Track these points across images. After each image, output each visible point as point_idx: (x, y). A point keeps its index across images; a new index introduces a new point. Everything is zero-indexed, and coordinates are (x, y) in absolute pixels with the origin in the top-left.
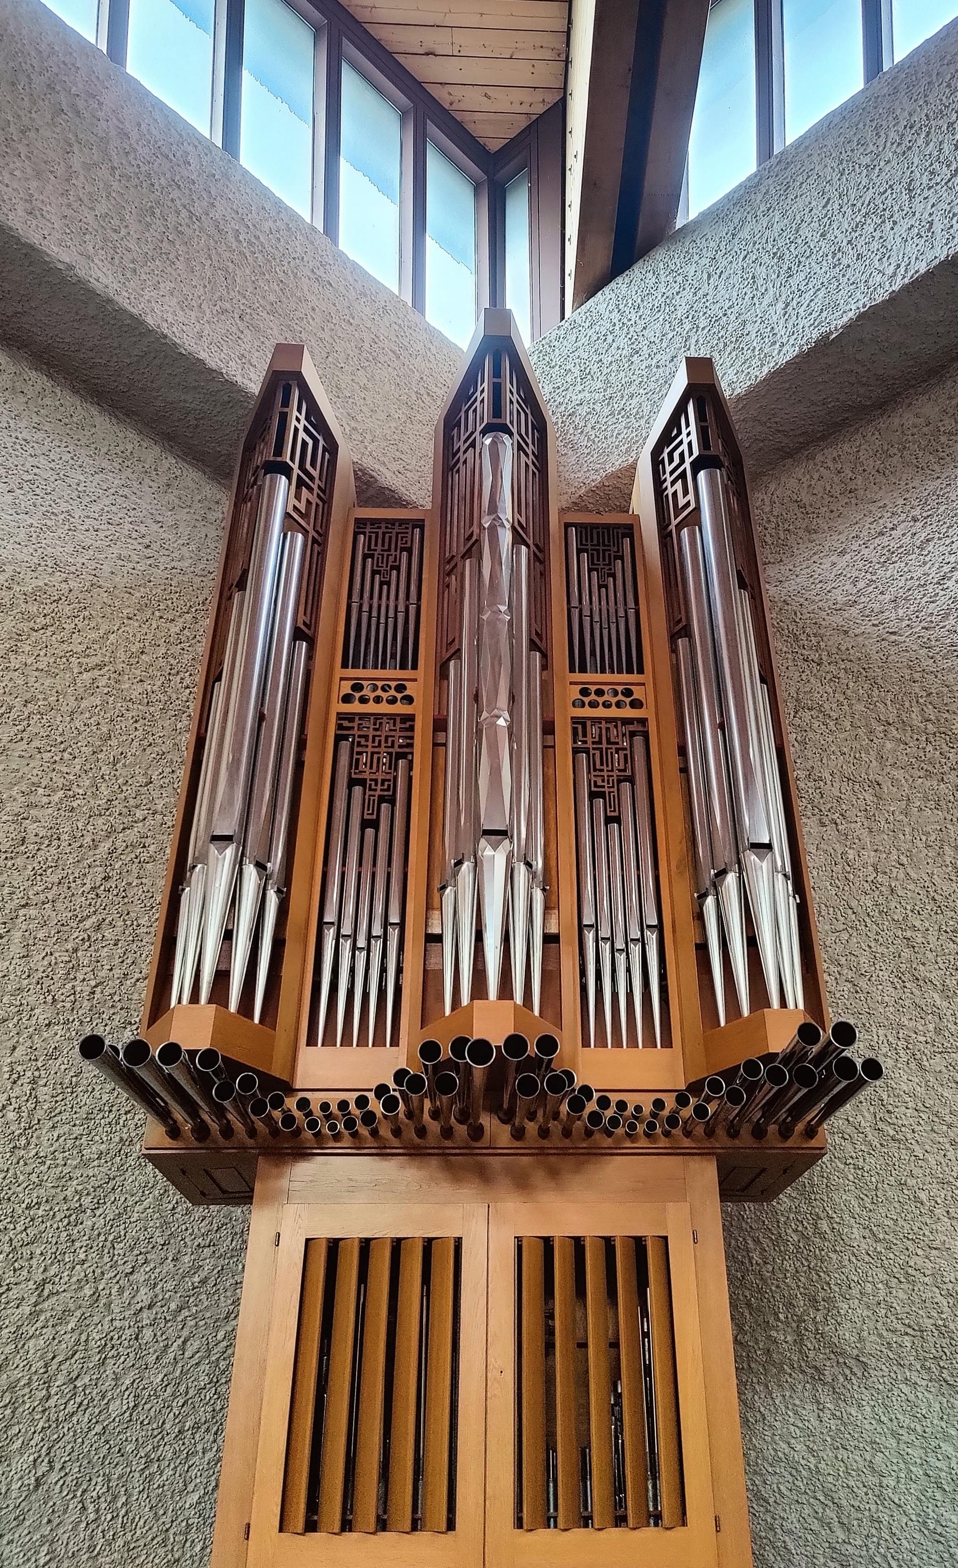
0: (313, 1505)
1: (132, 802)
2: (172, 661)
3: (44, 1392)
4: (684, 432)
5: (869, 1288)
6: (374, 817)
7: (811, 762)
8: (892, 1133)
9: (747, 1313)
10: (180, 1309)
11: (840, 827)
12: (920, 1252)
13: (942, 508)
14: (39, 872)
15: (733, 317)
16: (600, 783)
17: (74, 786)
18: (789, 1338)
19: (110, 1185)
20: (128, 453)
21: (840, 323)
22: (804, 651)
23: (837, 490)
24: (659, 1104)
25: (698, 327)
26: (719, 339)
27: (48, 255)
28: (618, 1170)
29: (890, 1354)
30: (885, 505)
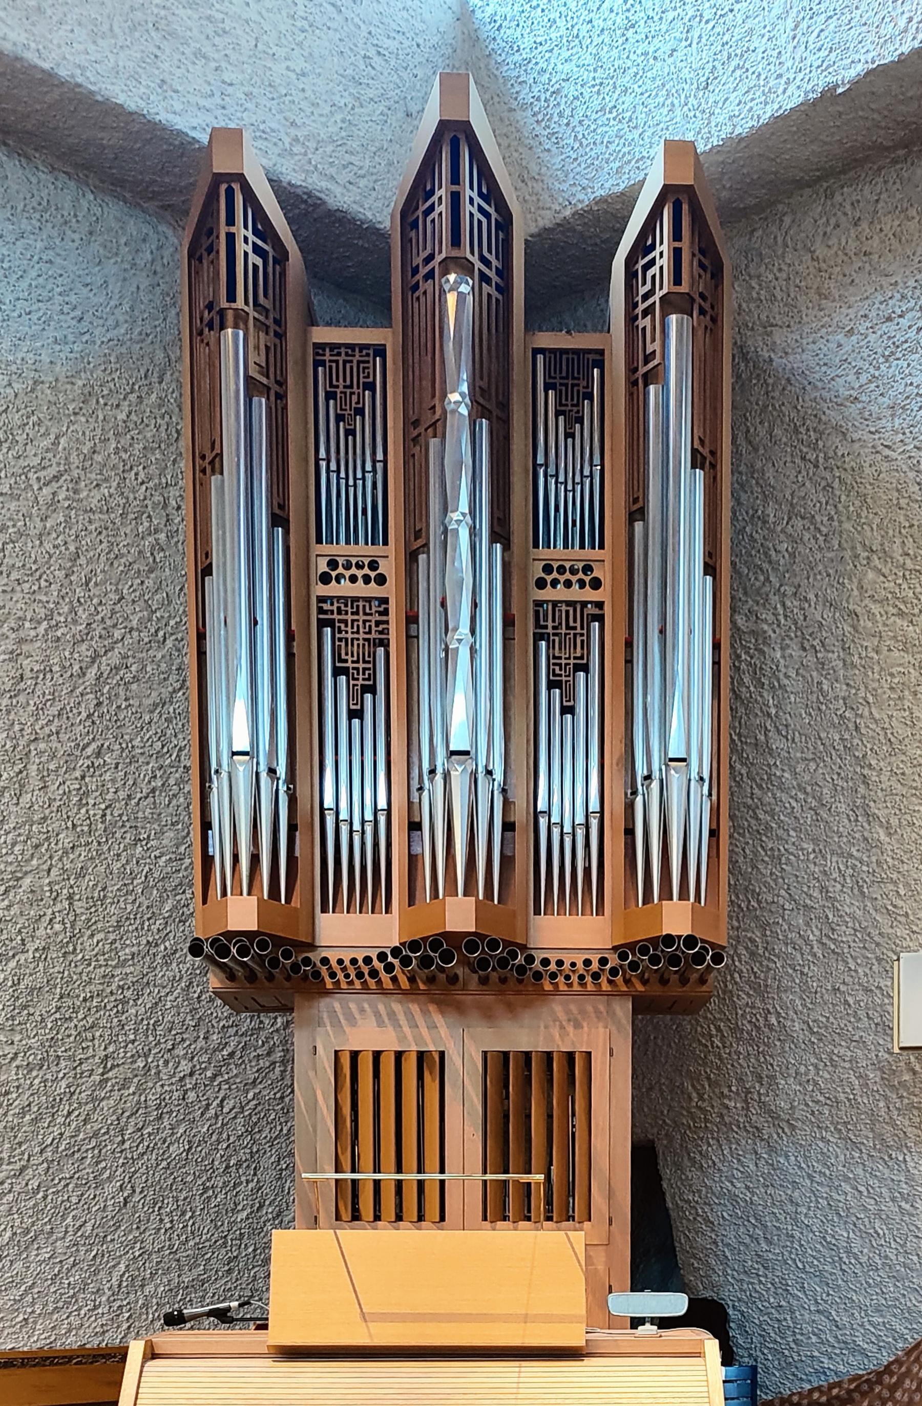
1: (109, 623)
2: (125, 456)
5: (802, 1069)
6: (359, 707)
7: (798, 579)
8: (833, 947)
10: (215, 1076)
11: (819, 655)
12: (843, 1043)
15: (740, 18)
16: (557, 671)
19: (145, 980)
20: (45, 203)
24: (587, 962)
25: (701, 15)
26: (723, 45)
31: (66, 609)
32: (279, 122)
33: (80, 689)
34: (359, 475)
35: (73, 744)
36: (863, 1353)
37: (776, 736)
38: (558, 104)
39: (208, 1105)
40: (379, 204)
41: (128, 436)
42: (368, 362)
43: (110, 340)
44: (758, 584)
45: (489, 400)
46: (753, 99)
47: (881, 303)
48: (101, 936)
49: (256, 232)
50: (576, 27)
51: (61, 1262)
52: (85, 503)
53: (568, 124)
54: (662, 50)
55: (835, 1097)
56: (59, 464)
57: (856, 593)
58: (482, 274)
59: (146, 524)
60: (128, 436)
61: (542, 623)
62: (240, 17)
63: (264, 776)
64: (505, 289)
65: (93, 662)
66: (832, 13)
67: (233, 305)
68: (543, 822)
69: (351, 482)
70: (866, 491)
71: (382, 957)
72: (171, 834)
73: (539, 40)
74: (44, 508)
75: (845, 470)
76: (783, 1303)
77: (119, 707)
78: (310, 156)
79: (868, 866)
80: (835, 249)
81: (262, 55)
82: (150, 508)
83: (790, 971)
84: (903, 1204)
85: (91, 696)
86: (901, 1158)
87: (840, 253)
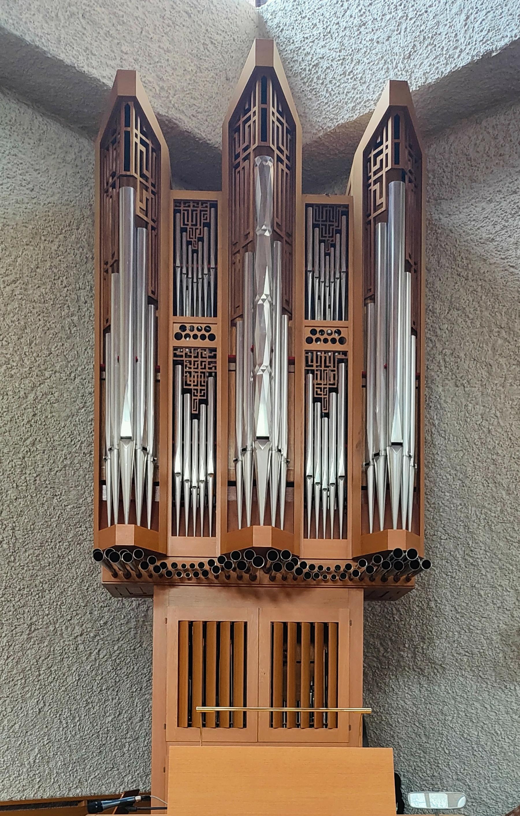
0: (190, 720)
1: (43, 367)
2: (55, 271)
3: (38, 673)
6: (197, 412)
7: (454, 345)
8: (471, 561)
11: (466, 389)
12: (477, 619)
16: (319, 392)
17: (11, 361)
18: (409, 655)
20: (13, 121)
21: (502, 43)
22: (458, 269)
25: (407, 16)
26: (420, 32)
28: (318, 594)
29: (457, 664)
31: (17, 359)
32: (153, 78)
33: (24, 406)
34: (200, 276)
35: (19, 438)
36: (486, 805)
37: (439, 437)
38: (317, 72)
39: (91, 653)
41: (58, 260)
42: (207, 211)
43: (49, 203)
44: (428, 349)
45: (281, 230)
46: (438, 62)
47: (510, 183)
48: (31, 551)
49: (142, 132)
50: (329, 27)
52: (31, 297)
53: (322, 83)
54: (382, 37)
55: (471, 651)
57: (490, 352)
58: (278, 158)
59: (67, 311)
60: (58, 260)
61: (310, 363)
62: (133, 15)
64: (292, 168)
65: (32, 390)
66: (490, 9)
67: (128, 173)
68: (309, 482)
69: (195, 280)
71: (211, 563)
72: (74, 492)
73: (306, 36)
74: (7, 298)
75: (485, 281)
76: (435, 774)
77: (47, 417)
78: (171, 98)
79: (495, 513)
80: (481, 153)
81: (145, 38)
82: (69, 302)
83: (444, 576)
84: (514, 716)
85: (30, 410)
86: (513, 688)
87: (484, 155)
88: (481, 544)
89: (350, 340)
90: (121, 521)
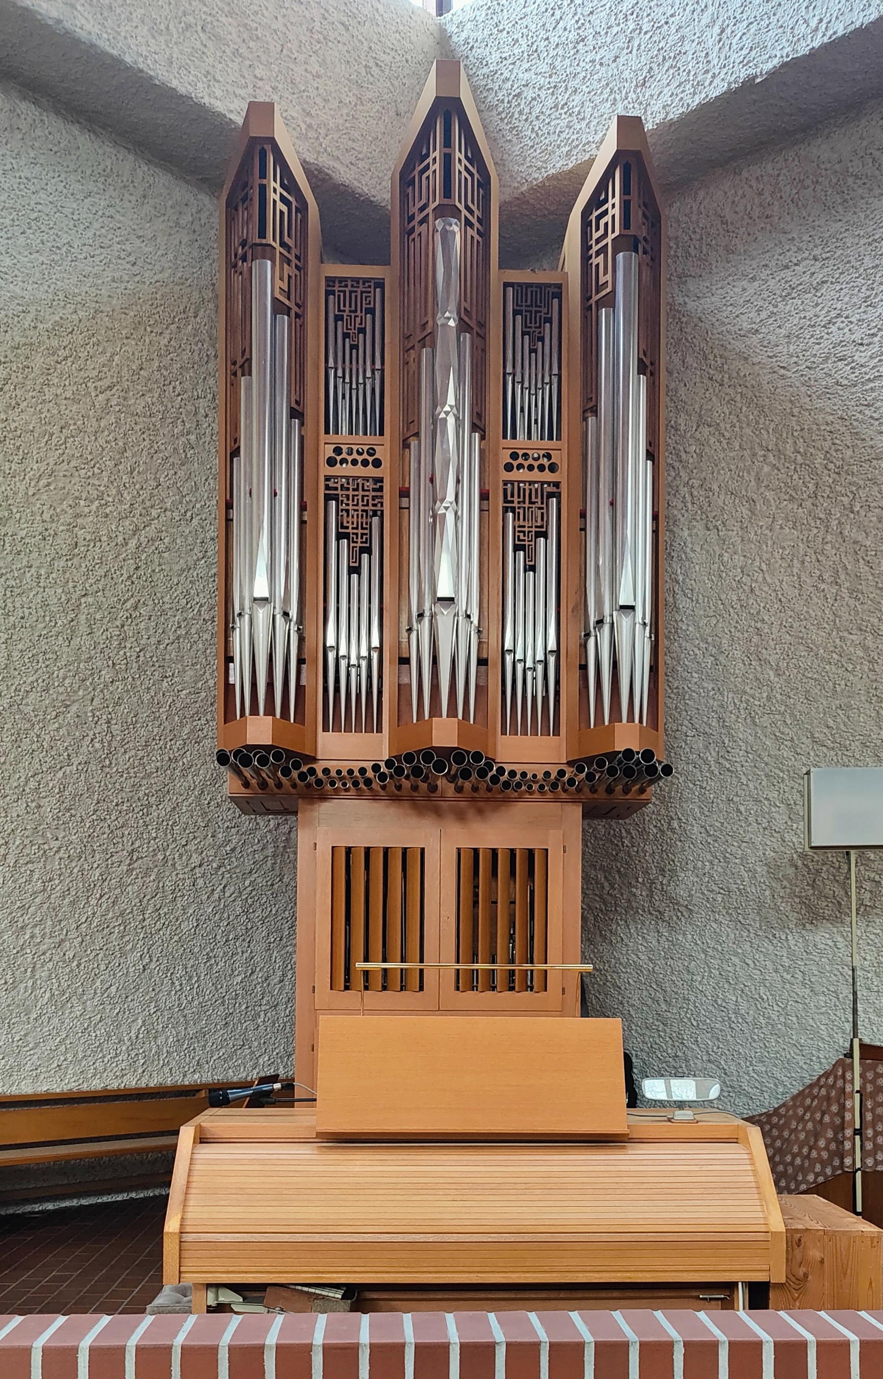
1: (148, 504)
4: (611, 202)
5: (700, 864)
6: (357, 565)
7: (704, 473)
8: (728, 766)
9: (617, 877)
11: (720, 533)
12: (735, 844)
13: (839, 252)
14: (90, 568)
15: (673, 29)
16: (522, 537)
17: (105, 495)
18: (644, 893)
20: (108, 170)
21: (769, 66)
22: (710, 370)
23: (756, 213)
25: (641, 28)
26: (659, 50)
27: (40, 14)
28: (521, 810)
30: (793, 239)
31: (114, 492)
33: (123, 556)
34: (361, 381)
35: (116, 599)
36: (747, 1095)
38: (519, 104)
40: (373, 182)
42: (370, 292)
43: (157, 281)
44: (670, 478)
45: (471, 319)
46: (683, 92)
47: (780, 255)
48: (133, 752)
51: (90, 1018)
53: (526, 120)
54: (607, 57)
55: (728, 888)
56: (112, 377)
57: (753, 483)
59: (181, 428)
60: (169, 358)
61: (509, 498)
62: (270, 27)
63: (279, 618)
64: (485, 234)
66: (753, 20)
67: (264, 241)
68: (509, 658)
69: (354, 386)
70: (764, 403)
71: (376, 768)
74: (100, 411)
76: (679, 1053)
77: (154, 571)
78: (321, 140)
80: (741, 214)
81: (286, 59)
82: (183, 415)
83: (691, 786)
85: (131, 561)
86: (783, 937)
88: (741, 743)
89: (563, 467)
90: (254, 711)
